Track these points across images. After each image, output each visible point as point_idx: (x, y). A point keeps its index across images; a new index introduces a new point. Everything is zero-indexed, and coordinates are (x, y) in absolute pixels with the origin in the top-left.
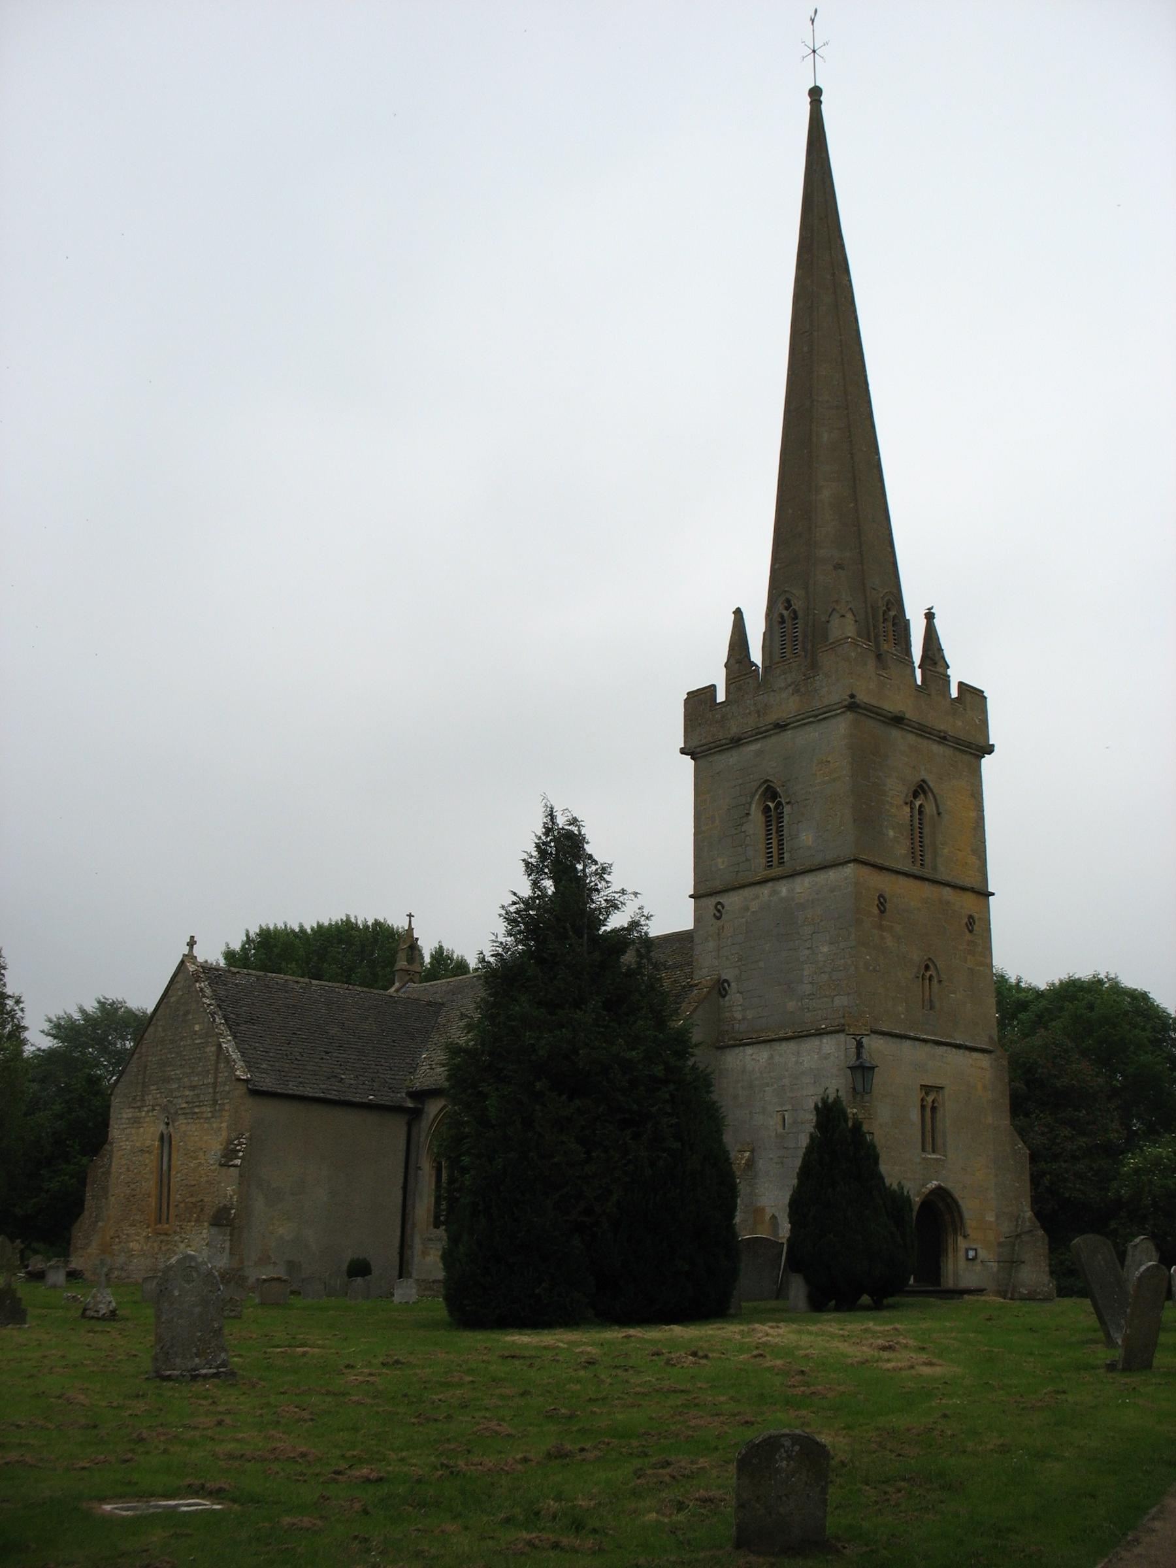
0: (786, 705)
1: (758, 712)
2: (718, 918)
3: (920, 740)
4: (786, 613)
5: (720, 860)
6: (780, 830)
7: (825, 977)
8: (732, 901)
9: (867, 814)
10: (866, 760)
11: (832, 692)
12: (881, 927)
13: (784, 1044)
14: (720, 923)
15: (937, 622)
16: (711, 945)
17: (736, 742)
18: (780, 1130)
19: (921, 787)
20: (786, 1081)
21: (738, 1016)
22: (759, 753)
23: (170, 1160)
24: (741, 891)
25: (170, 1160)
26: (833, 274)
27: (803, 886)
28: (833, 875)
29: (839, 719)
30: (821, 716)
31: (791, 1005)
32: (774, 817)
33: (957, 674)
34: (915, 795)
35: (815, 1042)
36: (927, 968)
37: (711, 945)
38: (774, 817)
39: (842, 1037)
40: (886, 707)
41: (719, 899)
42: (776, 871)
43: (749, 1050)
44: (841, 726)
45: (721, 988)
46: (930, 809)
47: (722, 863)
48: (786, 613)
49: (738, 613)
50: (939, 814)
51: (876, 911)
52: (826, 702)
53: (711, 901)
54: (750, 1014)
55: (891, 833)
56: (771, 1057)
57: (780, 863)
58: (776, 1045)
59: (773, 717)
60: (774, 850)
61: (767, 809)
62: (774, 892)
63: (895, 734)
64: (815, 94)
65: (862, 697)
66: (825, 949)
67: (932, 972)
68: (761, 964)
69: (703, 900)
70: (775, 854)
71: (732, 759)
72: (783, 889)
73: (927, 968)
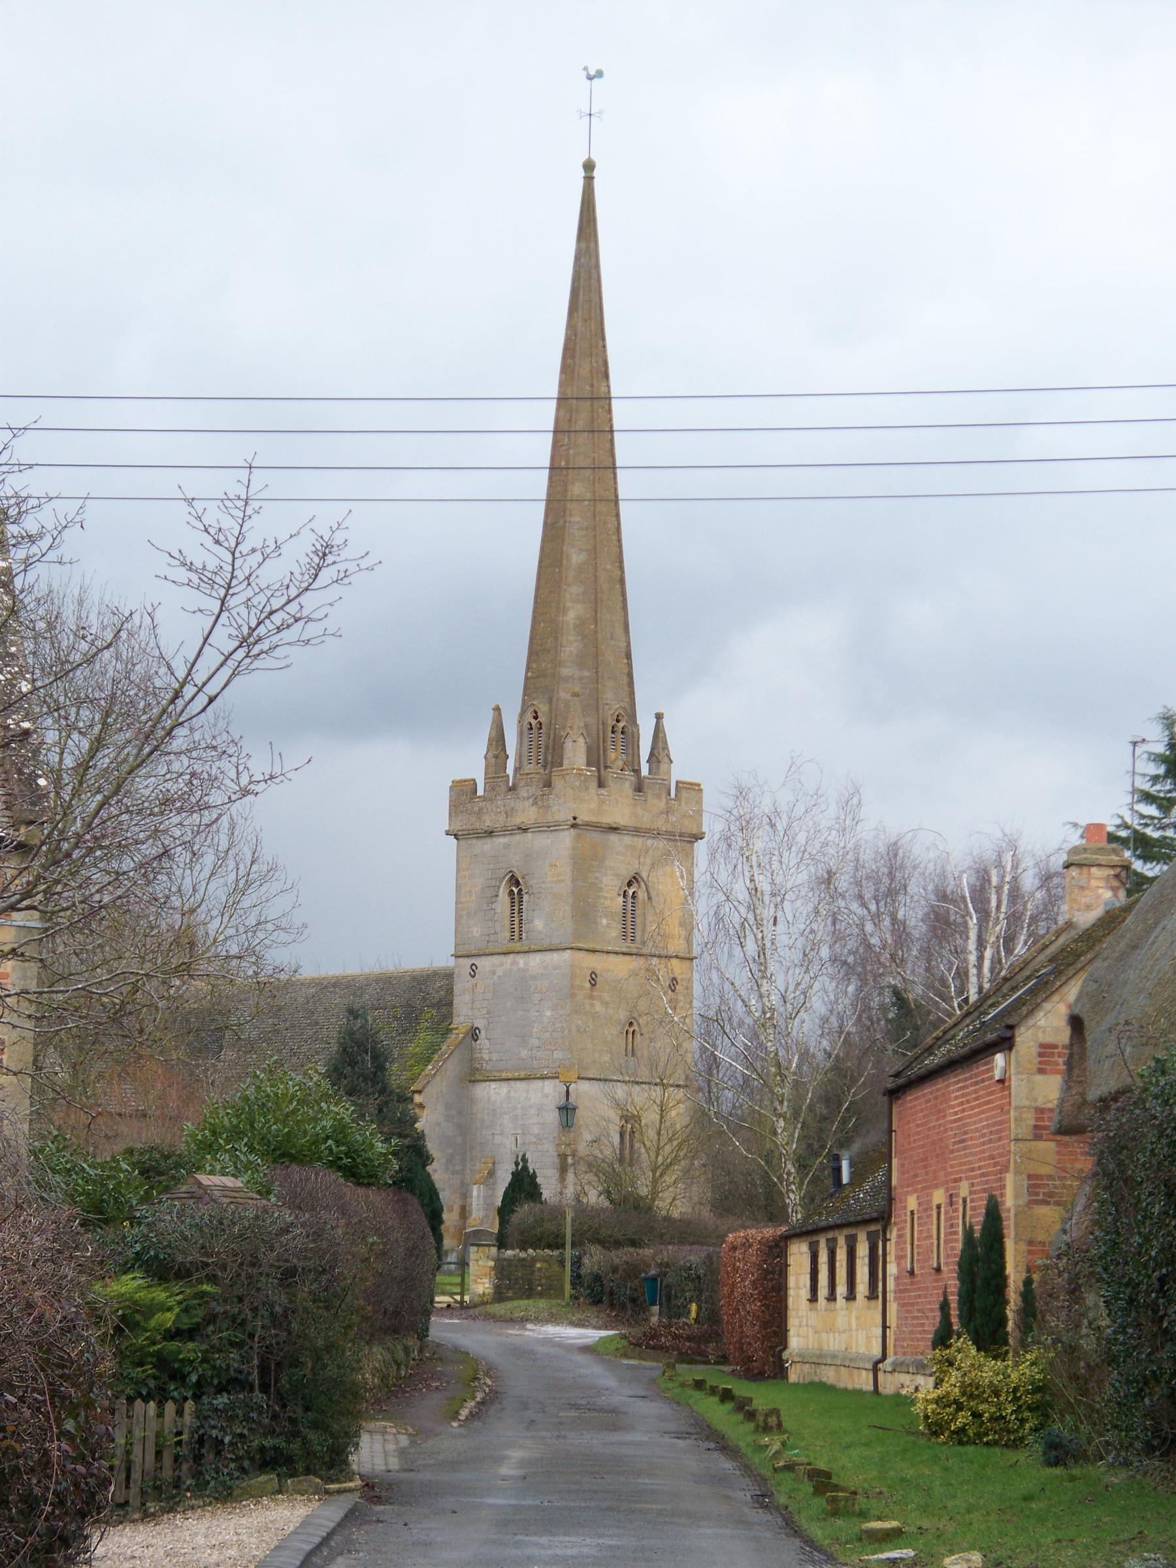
0: (527, 813)
1: (506, 813)
2: (473, 977)
3: (636, 839)
4: (534, 722)
5: (475, 929)
6: (520, 911)
7: (547, 1035)
8: (484, 964)
9: (584, 911)
10: (585, 866)
11: (561, 810)
12: (592, 997)
13: (518, 1083)
14: (473, 981)
15: (665, 721)
16: (467, 997)
17: (490, 833)
18: (514, 1148)
19: (634, 878)
20: (519, 1112)
21: (486, 1057)
22: (507, 846)
23: (627, 1045)
24: (490, 958)
25: (627, 1045)
26: (592, 386)
27: (535, 960)
28: (555, 956)
29: (566, 833)
30: (552, 827)
31: (524, 1053)
32: (516, 899)
33: (678, 772)
34: (629, 884)
35: (539, 1083)
36: (631, 1024)
37: (467, 997)
38: (516, 899)
39: (557, 1081)
40: (605, 821)
41: (474, 961)
42: (516, 946)
43: (493, 1085)
44: (567, 838)
45: (474, 1034)
46: (641, 895)
47: (476, 932)
48: (534, 722)
49: (497, 709)
50: (650, 898)
51: (588, 985)
52: (556, 818)
53: (467, 962)
54: (495, 1057)
55: (604, 921)
56: (509, 1092)
57: (518, 939)
58: (512, 1083)
59: (517, 820)
60: (516, 926)
61: (511, 893)
62: (515, 963)
63: (613, 838)
64: (589, 166)
65: (583, 817)
66: (548, 1014)
67: (635, 1027)
68: (503, 1018)
69: (461, 959)
70: (517, 930)
71: (486, 846)
72: (521, 960)
73: (631, 1024)
